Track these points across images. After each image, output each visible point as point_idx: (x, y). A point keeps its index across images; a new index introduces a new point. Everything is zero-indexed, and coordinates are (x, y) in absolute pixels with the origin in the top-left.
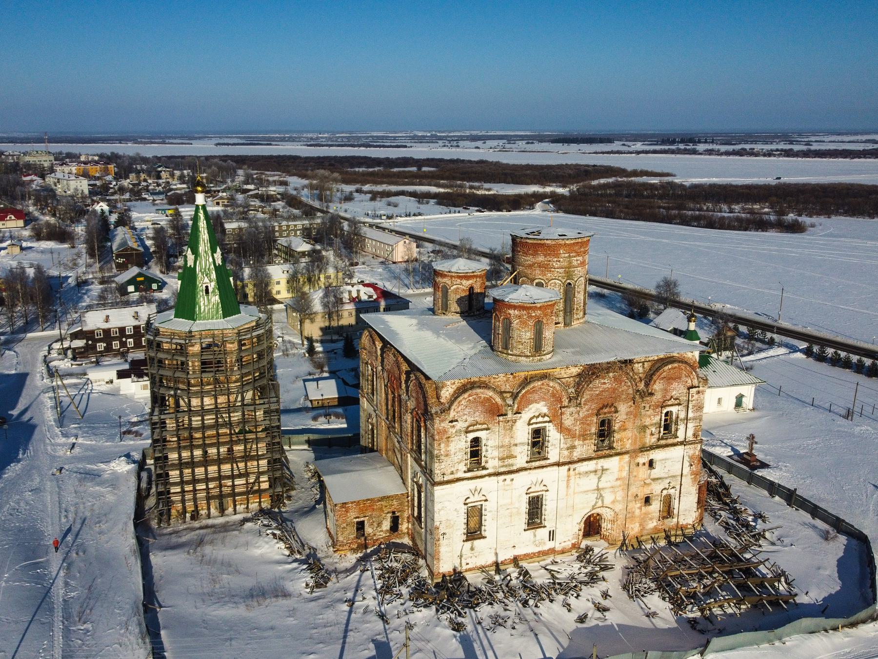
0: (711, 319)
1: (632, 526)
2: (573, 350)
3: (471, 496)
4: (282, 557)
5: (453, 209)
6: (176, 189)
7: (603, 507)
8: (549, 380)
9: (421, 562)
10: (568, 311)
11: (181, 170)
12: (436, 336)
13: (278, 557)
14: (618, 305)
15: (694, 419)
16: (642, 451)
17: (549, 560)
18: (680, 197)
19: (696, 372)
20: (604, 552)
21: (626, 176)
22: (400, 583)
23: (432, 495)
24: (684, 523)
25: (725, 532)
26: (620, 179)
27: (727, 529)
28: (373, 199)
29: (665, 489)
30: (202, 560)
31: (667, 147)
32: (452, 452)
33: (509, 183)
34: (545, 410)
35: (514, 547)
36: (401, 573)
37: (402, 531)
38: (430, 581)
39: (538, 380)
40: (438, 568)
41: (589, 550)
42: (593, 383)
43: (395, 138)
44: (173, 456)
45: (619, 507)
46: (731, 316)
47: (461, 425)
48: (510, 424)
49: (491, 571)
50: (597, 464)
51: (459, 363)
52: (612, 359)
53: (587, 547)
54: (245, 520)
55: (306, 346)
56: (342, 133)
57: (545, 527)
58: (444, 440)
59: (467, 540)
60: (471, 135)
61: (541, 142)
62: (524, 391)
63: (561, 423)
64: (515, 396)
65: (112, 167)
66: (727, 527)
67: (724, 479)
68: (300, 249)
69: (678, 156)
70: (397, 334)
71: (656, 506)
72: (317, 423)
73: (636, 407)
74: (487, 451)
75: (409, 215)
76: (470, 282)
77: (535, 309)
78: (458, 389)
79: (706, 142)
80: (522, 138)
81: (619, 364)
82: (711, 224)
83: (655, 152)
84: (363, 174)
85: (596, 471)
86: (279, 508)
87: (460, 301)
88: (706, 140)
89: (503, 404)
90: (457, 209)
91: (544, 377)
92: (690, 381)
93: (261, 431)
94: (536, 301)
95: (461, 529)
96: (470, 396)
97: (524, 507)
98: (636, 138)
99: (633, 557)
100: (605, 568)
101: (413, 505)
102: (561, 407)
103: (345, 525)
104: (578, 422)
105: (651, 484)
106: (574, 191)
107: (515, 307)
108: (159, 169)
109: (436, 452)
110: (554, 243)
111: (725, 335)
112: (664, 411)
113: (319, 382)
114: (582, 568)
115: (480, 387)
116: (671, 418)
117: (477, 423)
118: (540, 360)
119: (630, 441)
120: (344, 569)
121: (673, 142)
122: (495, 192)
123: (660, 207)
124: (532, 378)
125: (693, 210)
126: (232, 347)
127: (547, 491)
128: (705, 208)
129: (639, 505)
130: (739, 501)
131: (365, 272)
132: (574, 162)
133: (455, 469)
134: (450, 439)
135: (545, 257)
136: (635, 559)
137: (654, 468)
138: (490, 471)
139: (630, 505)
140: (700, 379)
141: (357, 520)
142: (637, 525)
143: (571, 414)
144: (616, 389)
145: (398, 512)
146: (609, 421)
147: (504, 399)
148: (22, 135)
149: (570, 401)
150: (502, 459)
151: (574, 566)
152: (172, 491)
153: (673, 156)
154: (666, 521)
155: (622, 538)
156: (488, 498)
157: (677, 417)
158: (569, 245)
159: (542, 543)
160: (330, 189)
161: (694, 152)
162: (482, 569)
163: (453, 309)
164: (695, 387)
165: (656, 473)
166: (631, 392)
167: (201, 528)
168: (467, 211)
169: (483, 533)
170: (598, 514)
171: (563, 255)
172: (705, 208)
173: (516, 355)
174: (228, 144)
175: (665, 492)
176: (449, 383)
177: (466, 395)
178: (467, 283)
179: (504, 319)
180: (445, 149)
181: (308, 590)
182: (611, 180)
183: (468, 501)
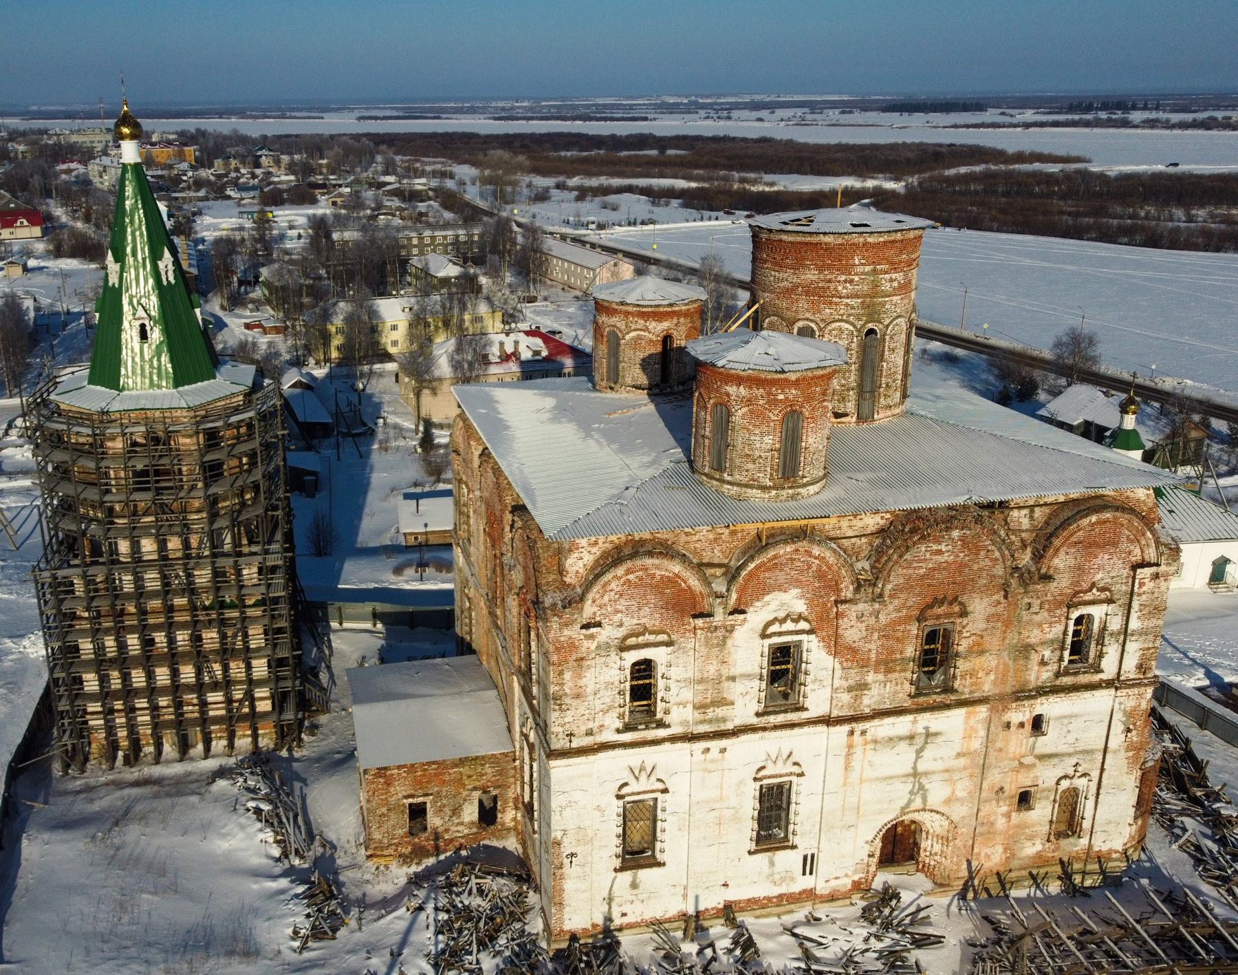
0: (1157, 405)
1: (989, 851)
2: (870, 475)
3: (631, 780)
4: (265, 861)
5: (706, 213)
6: (279, 183)
7: (924, 810)
8: (812, 541)
9: (532, 898)
10: (868, 390)
11: (290, 154)
12: (582, 435)
13: (258, 861)
14: (984, 376)
15: (1143, 633)
16: (1018, 699)
17: (801, 914)
18: (1099, 195)
19: (1153, 532)
20: (923, 902)
21: (1004, 163)
22: (482, 945)
23: (548, 775)
24: (1105, 848)
25: (1196, 866)
26: (993, 167)
27: (1198, 862)
28: (580, 198)
29: (1066, 777)
30: (113, 857)
31: (1077, 117)
32: (590, 690)
33: (805, 173)
34: (800, 607)
35: (726, 885)
36: (486, 923)
37: (503, 825)
38: (544, 945)
39: (786, 542)
40: (561, 920)
41: (889, 895)
42: (913, 551)
43: (631, 107)
44: (86, 646)
45: (959, 812)
46: (1200, 402)
47: (608, 633)
48: (720, 633)
49: (676, 929)
50: (915, 722)
51: (613, 496)
52: (960, 500)
53: (886, 888)
54: (221, 773)
55: (420, 435)
56: (551, 100)
57: (794, 847)
58: (572, 663)
59: (622, 869)
60: (753, 101)
61: (866, 110)
62: (752, 566)
63: (837, 636)
64: (732, 576)
65: (190, 151)
66: (1198, 856)
67: (1193, 746)
68: (441, 274)
69: (1096, 130)
70: (507, 428)
71: (1043, 812)
72: (401, 578)
73: (1009, 605)
74: (667, 689)
75: (635, 224)
76: (665, 325)
77: (787, 384)
78: (605, 555)
79: (1145, 108)
80: (833, 105)
81: (976, 511)
82: (1154, 241)
83: (1056, 124)
84: (573, 161)
85: (911, 737)
86: (290, 750)
87: (645, 364)
88: (1146, 104)
89: (705, 591)
90: (714, 214)
91: (801, 534)
92: (1137, 551)
93: (254, 606)
94: (786, 368)
95: (610, 846)
96: (628, 572)
97: (749, 806)
98: (1023, 103)
99: (986, 918)
100: (923, 942)
101: (523, 783)
102: (836, 602)
103: (384, 810)
104: (876, 635)
105: (1034, 765)
106: (913, 187)
107: (739, 380)
108: (259, 153)
109: (553, 689)
110: (840, 241)
111: (1185, 436)
112: (1075, 614)
113: (421, 502)
114: (872, 940)
115: (650, 554)
116: (1089, 629)
117: (645, 630)
118: (793, 497)
119: (992, 677)
120: (380, 897)
121: (1089, 108)
122: (782, 188)
123: (1062, 213)
124: (772, 536)
125: (1121, 217)
126: (186, 442)
127: (801, 775)
128: (1142, 214)
129: (1004, 809)
130: (1226, 795)
131: (545, 313)
132: (917, 141)
133: (597, 724)
134: (585, 663)
135: (821, 270)
136: (992, 923)
137: (1043, 734)
138: (676, 730)
139: (986, 810)
140: (1162, 548)
141: (410, 800)
142: (1000, 849)
143: (860, 618)
144: (966, 566)
145: (495, 788)
146: (947, 635)
147: (707, 582)
148: (87, 108)
149: (857, 590)
150: (701, 707)
151: (856, 931)
152: (90, 710)
153: (1087, 130)
154: (1064, 843)
155: (965, 873)
156: (668, 785)
157: (1104, 629)
158: (874, 246)
159: (788, 878)
160: (515, 184)
161: (1125, 124)
162: (657, 925)
163: (629, 381)
164: (1150, 565)
165: (1047, 743)
166: (1000, 573)
167: (137, 784)
168: (731, 217)
169: (658, 855)
170: (913, 822)
171: (860, 269)
172: (1142, 214)
173: (739, 485)
174: (376, 118)
175: (1065, 784)
176: (583, 542)
177: (620, 571)
178: (658, 328)
179: (716, 405)
180: (709, 122)
181: (296, 944)
182: (978, 168)
183: (625, 791)
